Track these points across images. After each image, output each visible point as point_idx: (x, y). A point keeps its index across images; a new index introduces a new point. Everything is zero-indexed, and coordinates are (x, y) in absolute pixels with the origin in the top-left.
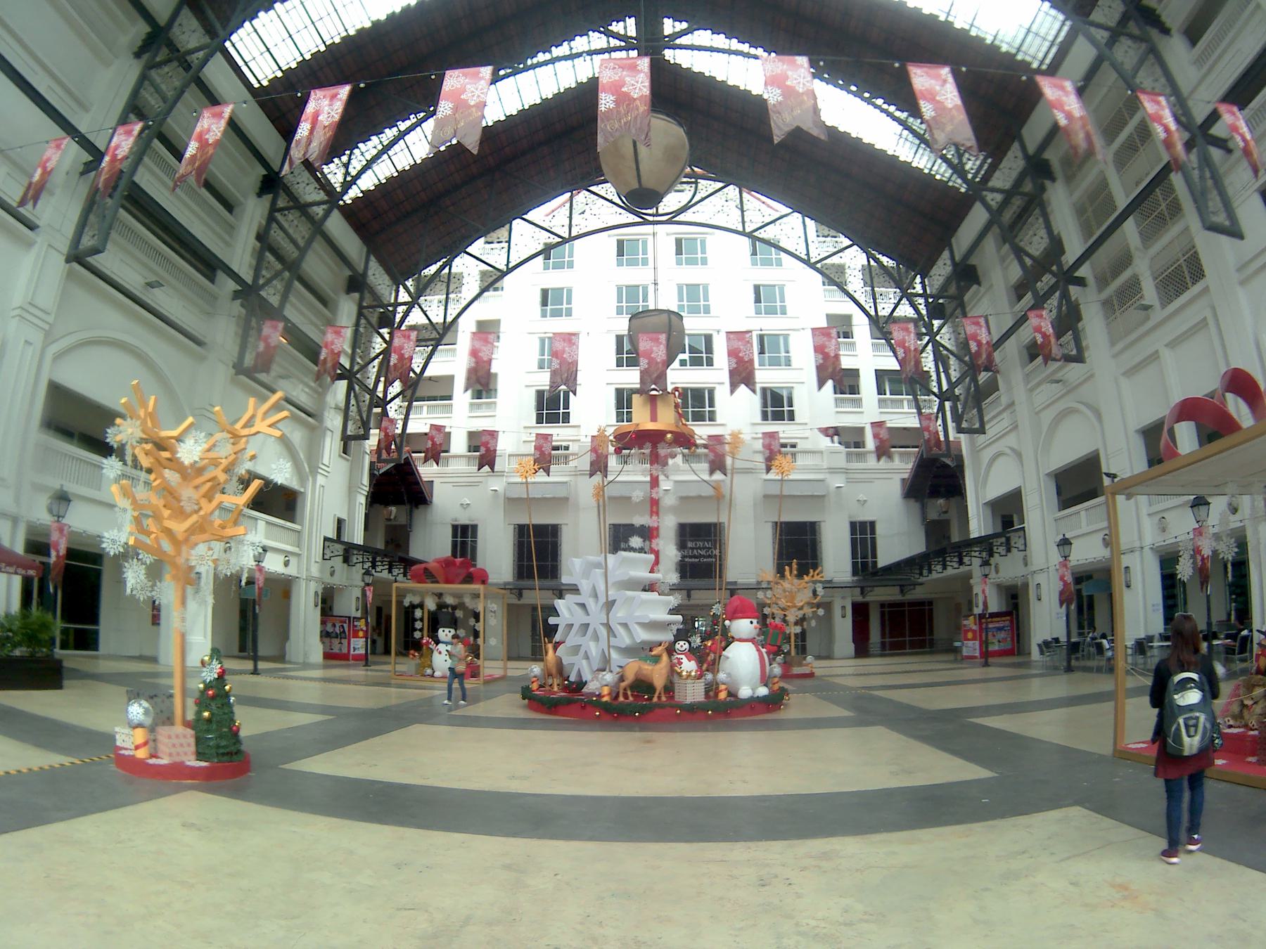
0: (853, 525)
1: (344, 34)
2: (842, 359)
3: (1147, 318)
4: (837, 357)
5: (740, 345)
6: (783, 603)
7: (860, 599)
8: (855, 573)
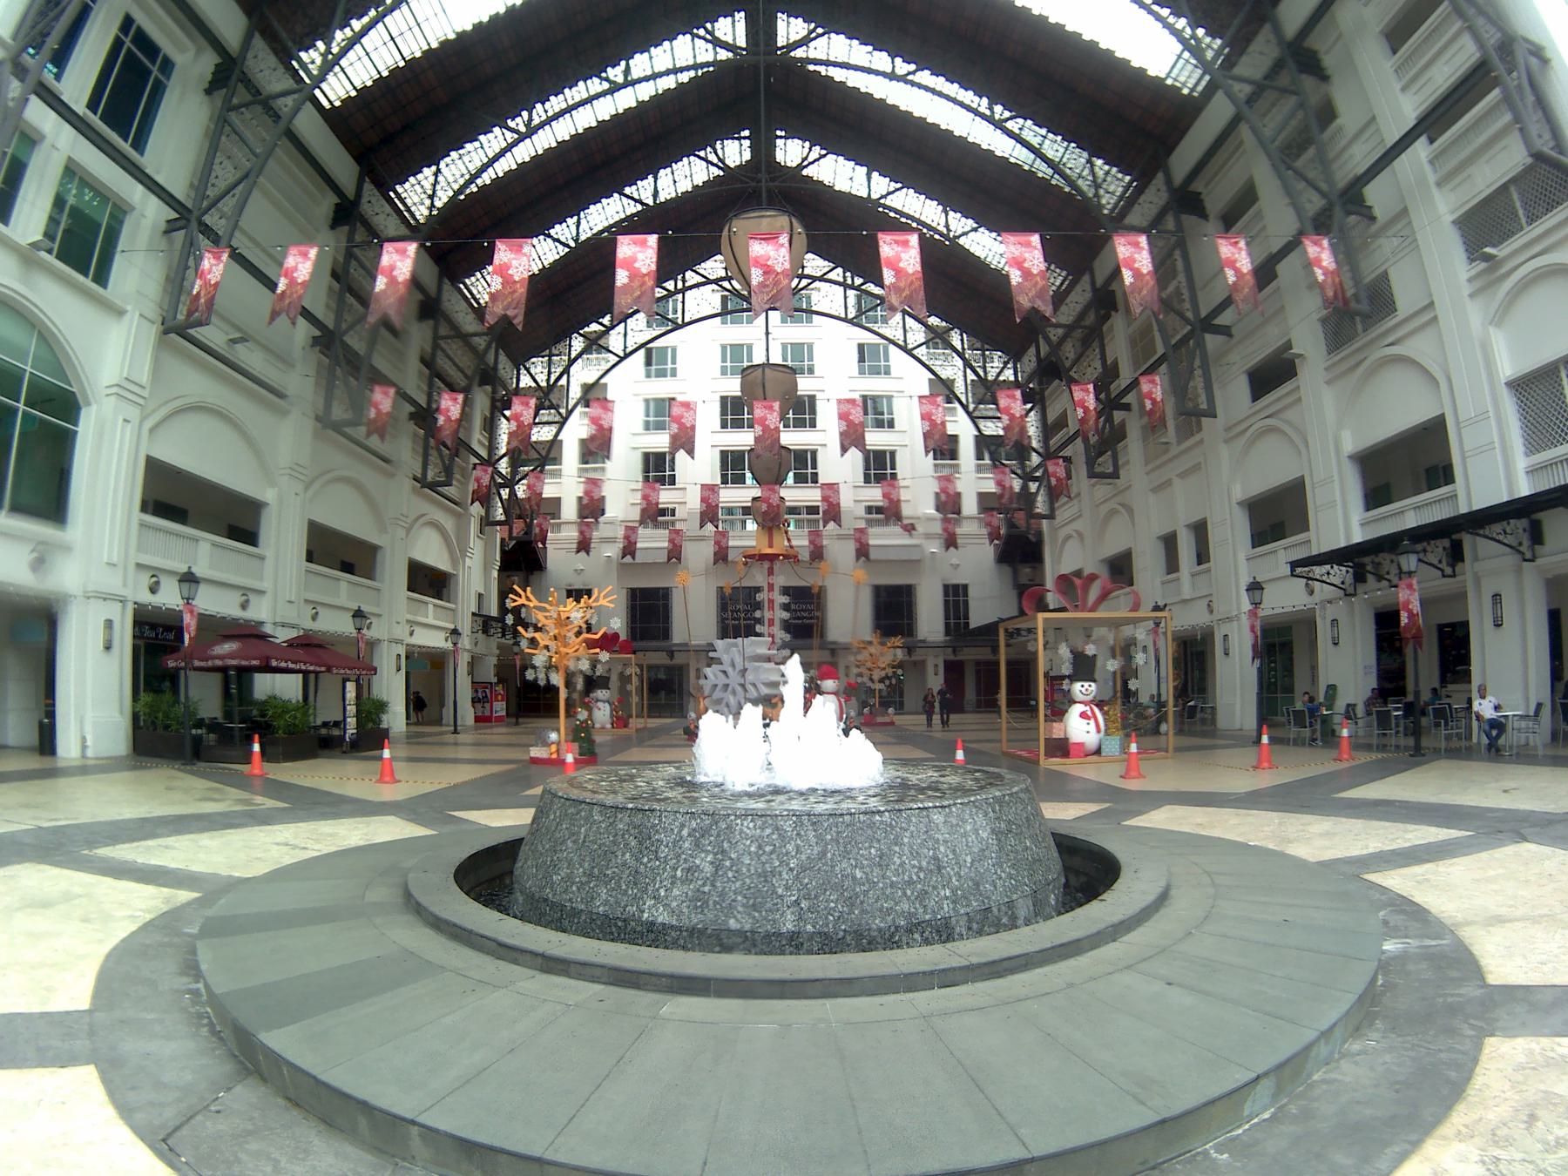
0: (946, 587)
1: (425, 47)
2: (948, 425)
3: (1167, 450)
4: (943, 423)
5: (829, 493)
6: (869, 665)
7: (952, 657)
8: (947, 633)
